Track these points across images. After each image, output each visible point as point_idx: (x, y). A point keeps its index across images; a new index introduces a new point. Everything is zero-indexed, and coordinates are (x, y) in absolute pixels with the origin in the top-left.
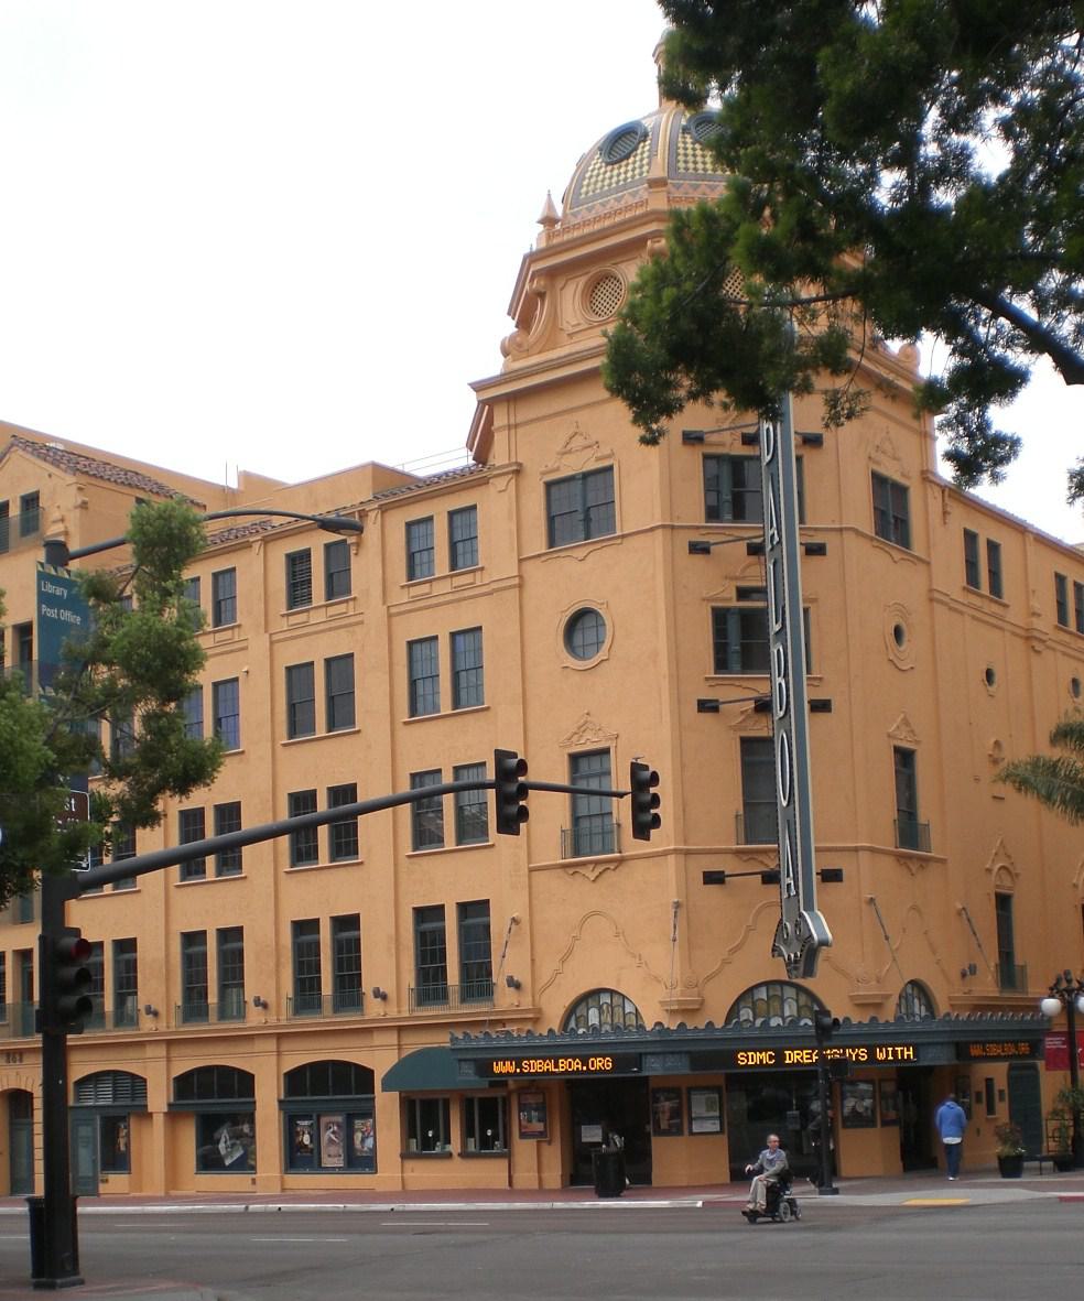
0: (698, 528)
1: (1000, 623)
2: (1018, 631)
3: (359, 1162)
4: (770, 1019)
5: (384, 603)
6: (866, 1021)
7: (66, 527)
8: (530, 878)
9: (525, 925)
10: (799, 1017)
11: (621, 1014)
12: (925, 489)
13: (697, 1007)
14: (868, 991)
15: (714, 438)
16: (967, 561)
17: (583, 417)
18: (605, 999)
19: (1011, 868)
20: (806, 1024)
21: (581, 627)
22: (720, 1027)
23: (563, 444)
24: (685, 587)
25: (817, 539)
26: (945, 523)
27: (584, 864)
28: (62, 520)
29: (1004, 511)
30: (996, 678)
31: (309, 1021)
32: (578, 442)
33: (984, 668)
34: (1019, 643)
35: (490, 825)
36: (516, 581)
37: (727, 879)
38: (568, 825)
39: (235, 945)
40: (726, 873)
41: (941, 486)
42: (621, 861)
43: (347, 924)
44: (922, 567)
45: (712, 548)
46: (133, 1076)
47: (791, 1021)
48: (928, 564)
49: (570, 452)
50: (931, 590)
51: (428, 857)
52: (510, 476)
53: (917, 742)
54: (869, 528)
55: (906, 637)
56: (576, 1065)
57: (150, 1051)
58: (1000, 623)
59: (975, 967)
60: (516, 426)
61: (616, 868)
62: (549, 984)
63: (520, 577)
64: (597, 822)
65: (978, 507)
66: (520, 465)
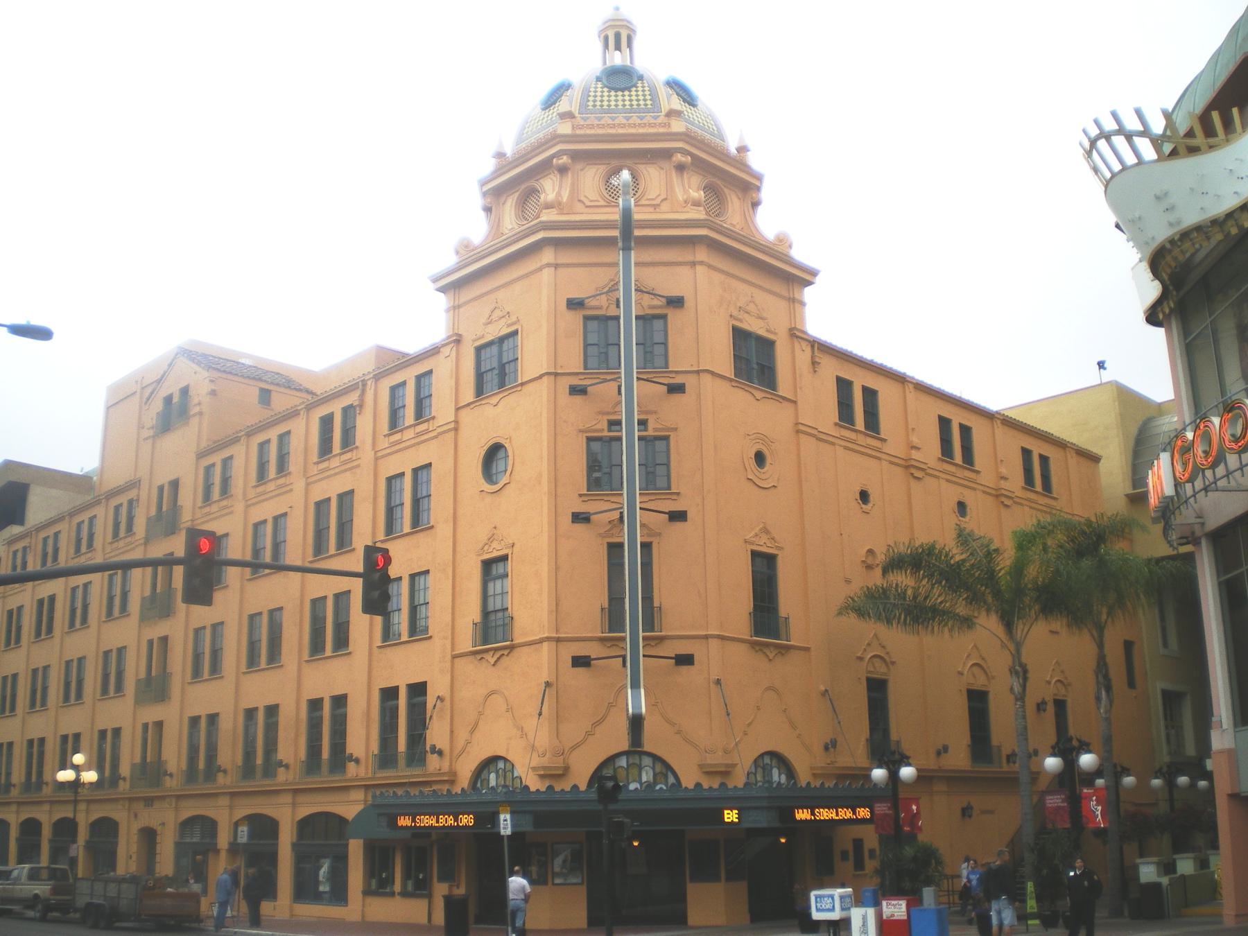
0: (577, 374)
1: (878, 455)
2: (896, 460)
4: (629, 784)
5: (373, 449)
6: (543, 789)
7: (201, 409)
9: (447, 702)
10: (655, 783)
11: (511, 777)
12: (793, 344)
13: (561, 772)
14: (717, 759)
15: (593, 303)
16: (941, 438)
17: (500, 295)
18: (501, 765)
19: (1065, 681)
20: (661, 788)
22: (584, 790)
23: (487, 316)
24: (565, 422)
25: (679, 380)
26: (815, 371)
27: (487, 651)
31: (316, 781)
32: (498, 313)
33: (858, 489)
34: (899, 470)
36: (452, 425)
37: (592, 662)
38: (478, 619)
40: (592, 657)
41: (809, 342)
43: (340, 701)
44: (790, 406)
45: (589, 389)
47: (647, 786)
48: (795, 402)
51: (405, 645)
52: (453, 345)
53: (780, 548)
54: (727, 368)
55: (769, 460)
56: (451, 821)
58: (878, 455)
59: (836, 741)
60: (459, 306)
61: (509, 653)
62: (463, 750)
63: (456, 422)
64: (500, 615)
65: (851, 359)
66: (460, 335)
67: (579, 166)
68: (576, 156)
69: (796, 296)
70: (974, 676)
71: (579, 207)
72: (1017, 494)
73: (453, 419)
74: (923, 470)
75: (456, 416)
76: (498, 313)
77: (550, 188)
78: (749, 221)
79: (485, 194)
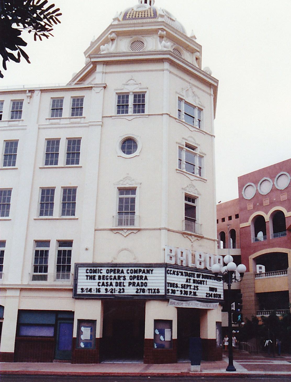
3: (204, 284)
5: (37, 123)
8: (95, 232)
27: (122, 230)
39: (118, 109)
49: (127, 85)
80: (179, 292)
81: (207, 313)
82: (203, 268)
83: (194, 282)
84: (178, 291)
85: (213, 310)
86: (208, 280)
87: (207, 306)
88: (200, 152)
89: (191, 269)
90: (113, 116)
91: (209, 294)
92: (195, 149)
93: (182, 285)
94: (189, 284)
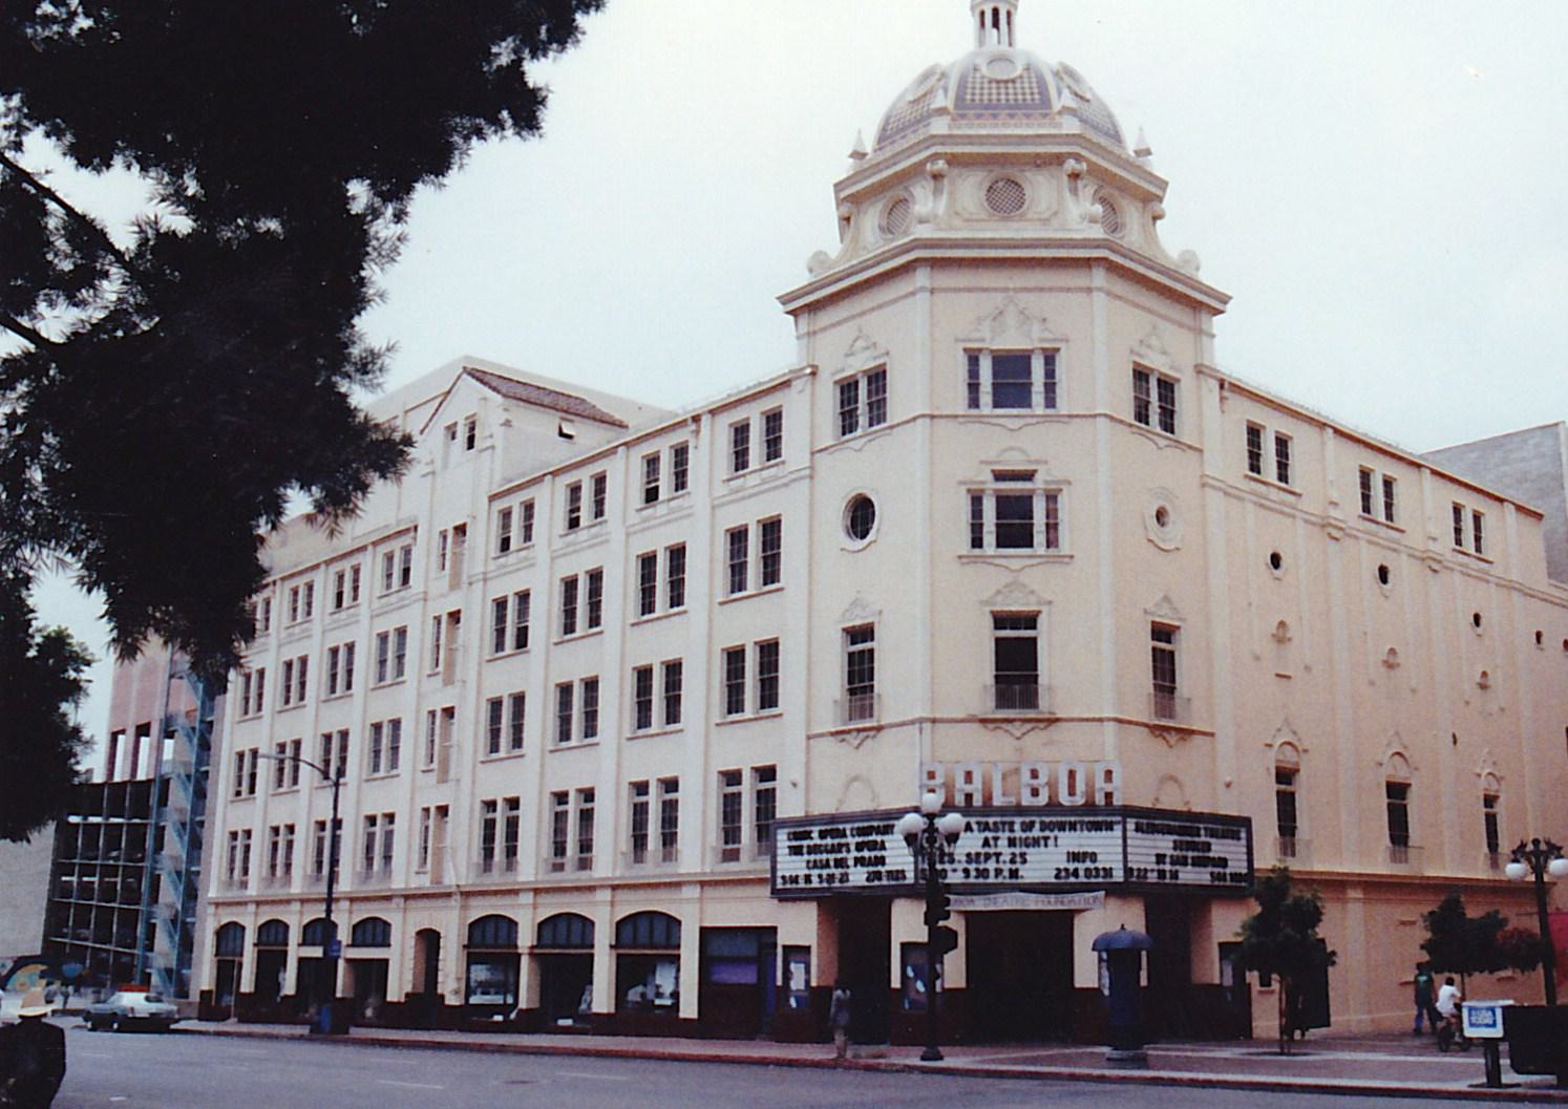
2: (1313, 519)
5: (624, 522)
19: (1404, 753)
21: (861, 516)
27: (849, 732)
28: (491, 436)
29: (1366, 435)
30: (1283, 563)
32: (860, 344)
34: (1316, 530)
35: (1010, 711)
36: (807, 472)
42: (879, 729)
46: (584, 919)
50: (1203, 476)
57: (394, 904)
60: (815, 333)
63: (812, 468)
67: (956, 171)
68: (954, 160)
69: (1204, 327)
70: (1395, 768)
71: (957, 222)
72: (1350, 524)
73: (808, 464)
74: (1341, 529)
75: (812, 460)
76: (860, 344)
77: (924, 200)
78: (1152, 238)
79: (840, 202)
80: (961, 874)
81: (1210, 911)
82: (1044, 803)
83: (1012, 842)
84: (955, 870)
85: (1085, 914)
86: (1061, 834)
87: (1062, 903)
88: (1046, 482)
89: (1003, 811)
90: (832, 446)
91: (1066, 870)
92: (1033, 475)
93: (969, 855)
94: (992, 850)
